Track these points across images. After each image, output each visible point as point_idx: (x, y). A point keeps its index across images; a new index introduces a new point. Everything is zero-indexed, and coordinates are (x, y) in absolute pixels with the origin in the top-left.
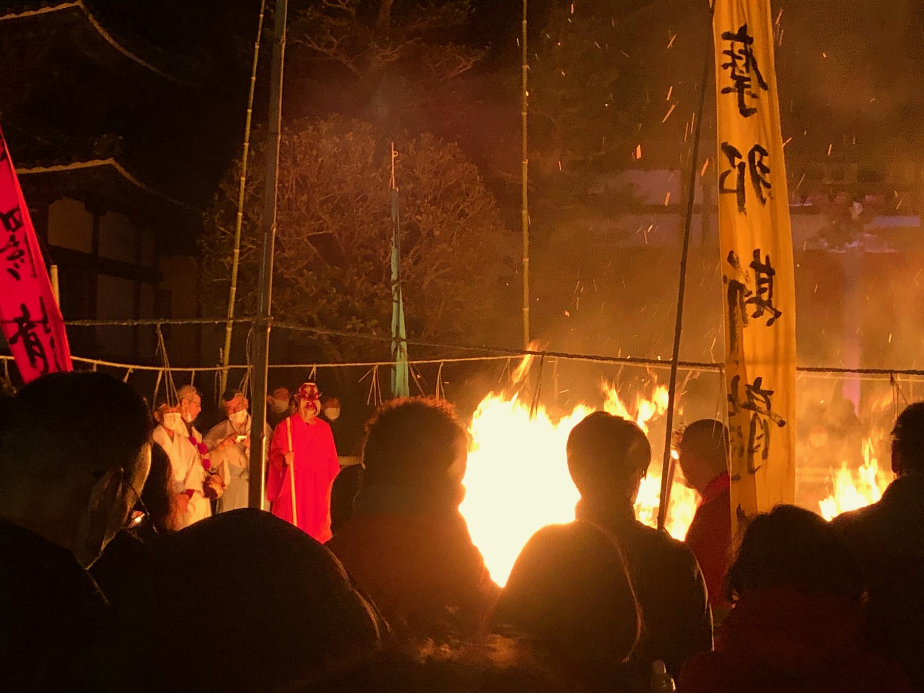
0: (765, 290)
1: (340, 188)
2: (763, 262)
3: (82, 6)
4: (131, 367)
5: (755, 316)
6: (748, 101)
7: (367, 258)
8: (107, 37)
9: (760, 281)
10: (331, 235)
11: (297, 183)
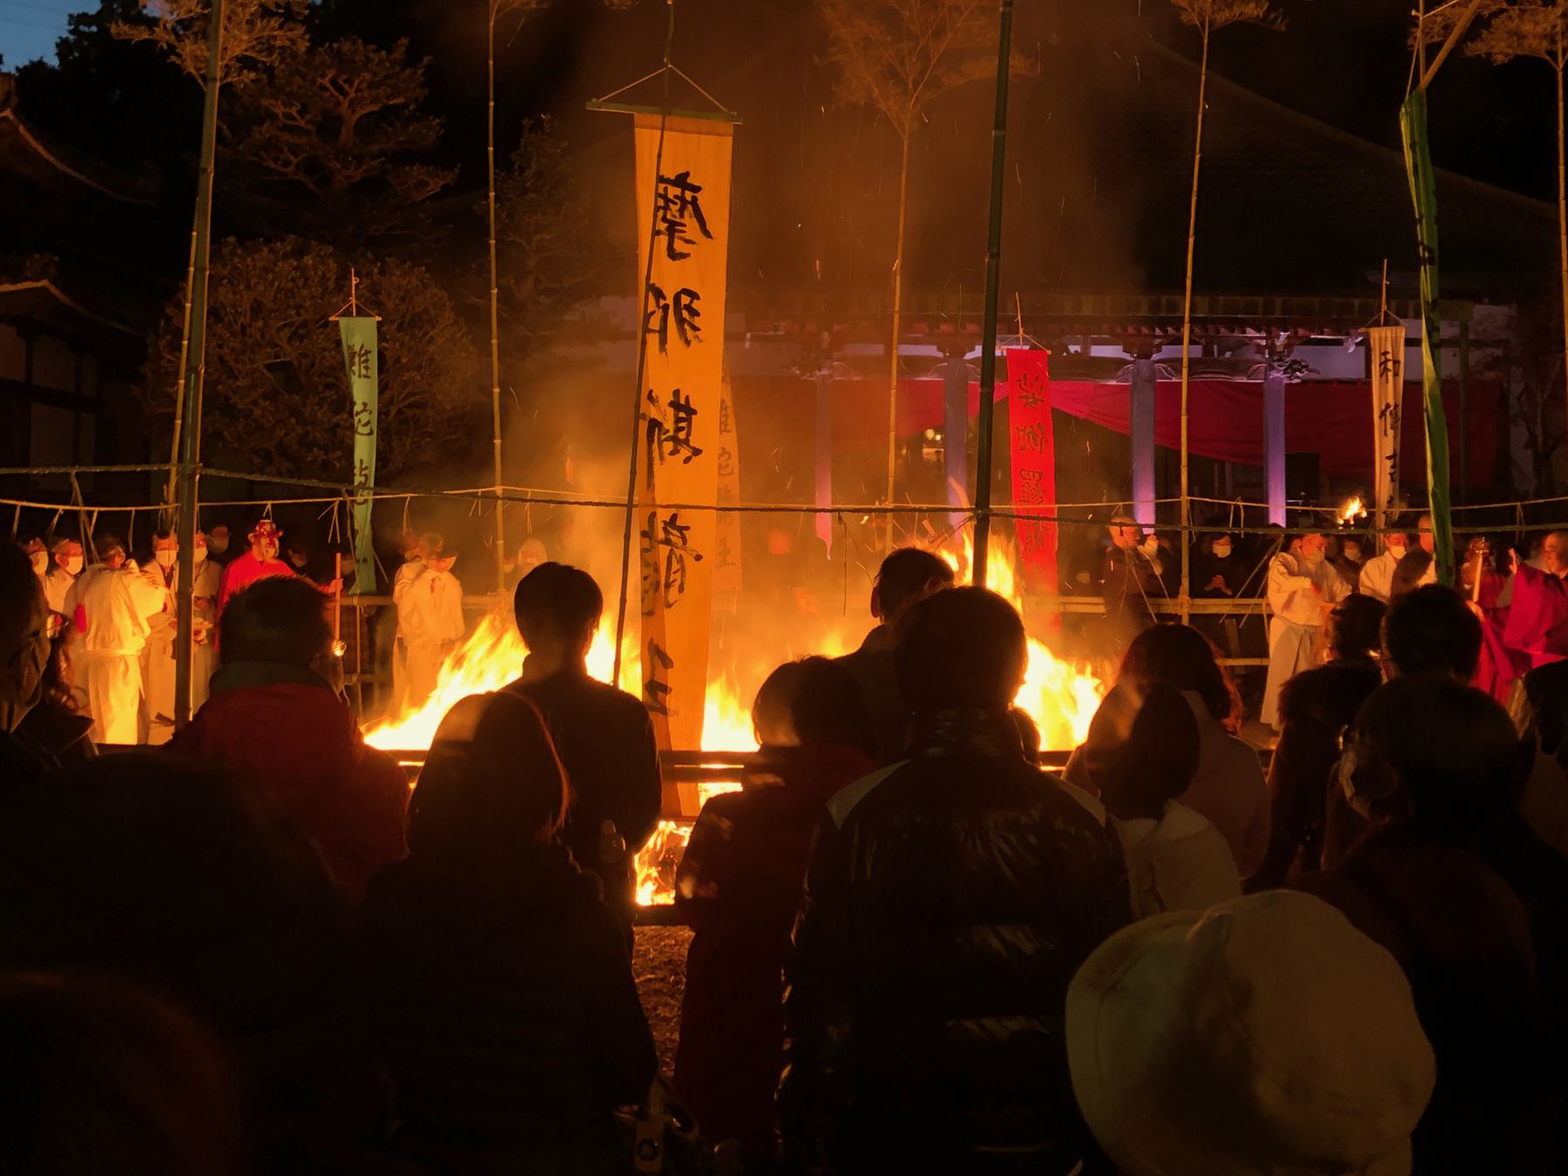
0: (683, 429)
1: (298, 314)
2: (682, 402)
3: (11, 117)
4: (61, 508)
5: (672, 453)
6: (679, 246)
7: (329, 386)
8: (40, 149)
9: (678, 420)
10: (290, 363)
11: (252, 309)
